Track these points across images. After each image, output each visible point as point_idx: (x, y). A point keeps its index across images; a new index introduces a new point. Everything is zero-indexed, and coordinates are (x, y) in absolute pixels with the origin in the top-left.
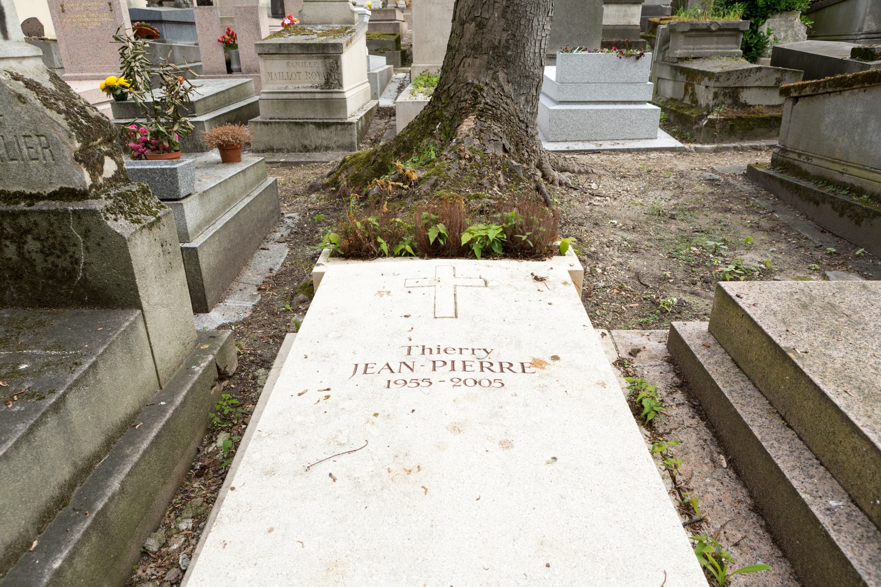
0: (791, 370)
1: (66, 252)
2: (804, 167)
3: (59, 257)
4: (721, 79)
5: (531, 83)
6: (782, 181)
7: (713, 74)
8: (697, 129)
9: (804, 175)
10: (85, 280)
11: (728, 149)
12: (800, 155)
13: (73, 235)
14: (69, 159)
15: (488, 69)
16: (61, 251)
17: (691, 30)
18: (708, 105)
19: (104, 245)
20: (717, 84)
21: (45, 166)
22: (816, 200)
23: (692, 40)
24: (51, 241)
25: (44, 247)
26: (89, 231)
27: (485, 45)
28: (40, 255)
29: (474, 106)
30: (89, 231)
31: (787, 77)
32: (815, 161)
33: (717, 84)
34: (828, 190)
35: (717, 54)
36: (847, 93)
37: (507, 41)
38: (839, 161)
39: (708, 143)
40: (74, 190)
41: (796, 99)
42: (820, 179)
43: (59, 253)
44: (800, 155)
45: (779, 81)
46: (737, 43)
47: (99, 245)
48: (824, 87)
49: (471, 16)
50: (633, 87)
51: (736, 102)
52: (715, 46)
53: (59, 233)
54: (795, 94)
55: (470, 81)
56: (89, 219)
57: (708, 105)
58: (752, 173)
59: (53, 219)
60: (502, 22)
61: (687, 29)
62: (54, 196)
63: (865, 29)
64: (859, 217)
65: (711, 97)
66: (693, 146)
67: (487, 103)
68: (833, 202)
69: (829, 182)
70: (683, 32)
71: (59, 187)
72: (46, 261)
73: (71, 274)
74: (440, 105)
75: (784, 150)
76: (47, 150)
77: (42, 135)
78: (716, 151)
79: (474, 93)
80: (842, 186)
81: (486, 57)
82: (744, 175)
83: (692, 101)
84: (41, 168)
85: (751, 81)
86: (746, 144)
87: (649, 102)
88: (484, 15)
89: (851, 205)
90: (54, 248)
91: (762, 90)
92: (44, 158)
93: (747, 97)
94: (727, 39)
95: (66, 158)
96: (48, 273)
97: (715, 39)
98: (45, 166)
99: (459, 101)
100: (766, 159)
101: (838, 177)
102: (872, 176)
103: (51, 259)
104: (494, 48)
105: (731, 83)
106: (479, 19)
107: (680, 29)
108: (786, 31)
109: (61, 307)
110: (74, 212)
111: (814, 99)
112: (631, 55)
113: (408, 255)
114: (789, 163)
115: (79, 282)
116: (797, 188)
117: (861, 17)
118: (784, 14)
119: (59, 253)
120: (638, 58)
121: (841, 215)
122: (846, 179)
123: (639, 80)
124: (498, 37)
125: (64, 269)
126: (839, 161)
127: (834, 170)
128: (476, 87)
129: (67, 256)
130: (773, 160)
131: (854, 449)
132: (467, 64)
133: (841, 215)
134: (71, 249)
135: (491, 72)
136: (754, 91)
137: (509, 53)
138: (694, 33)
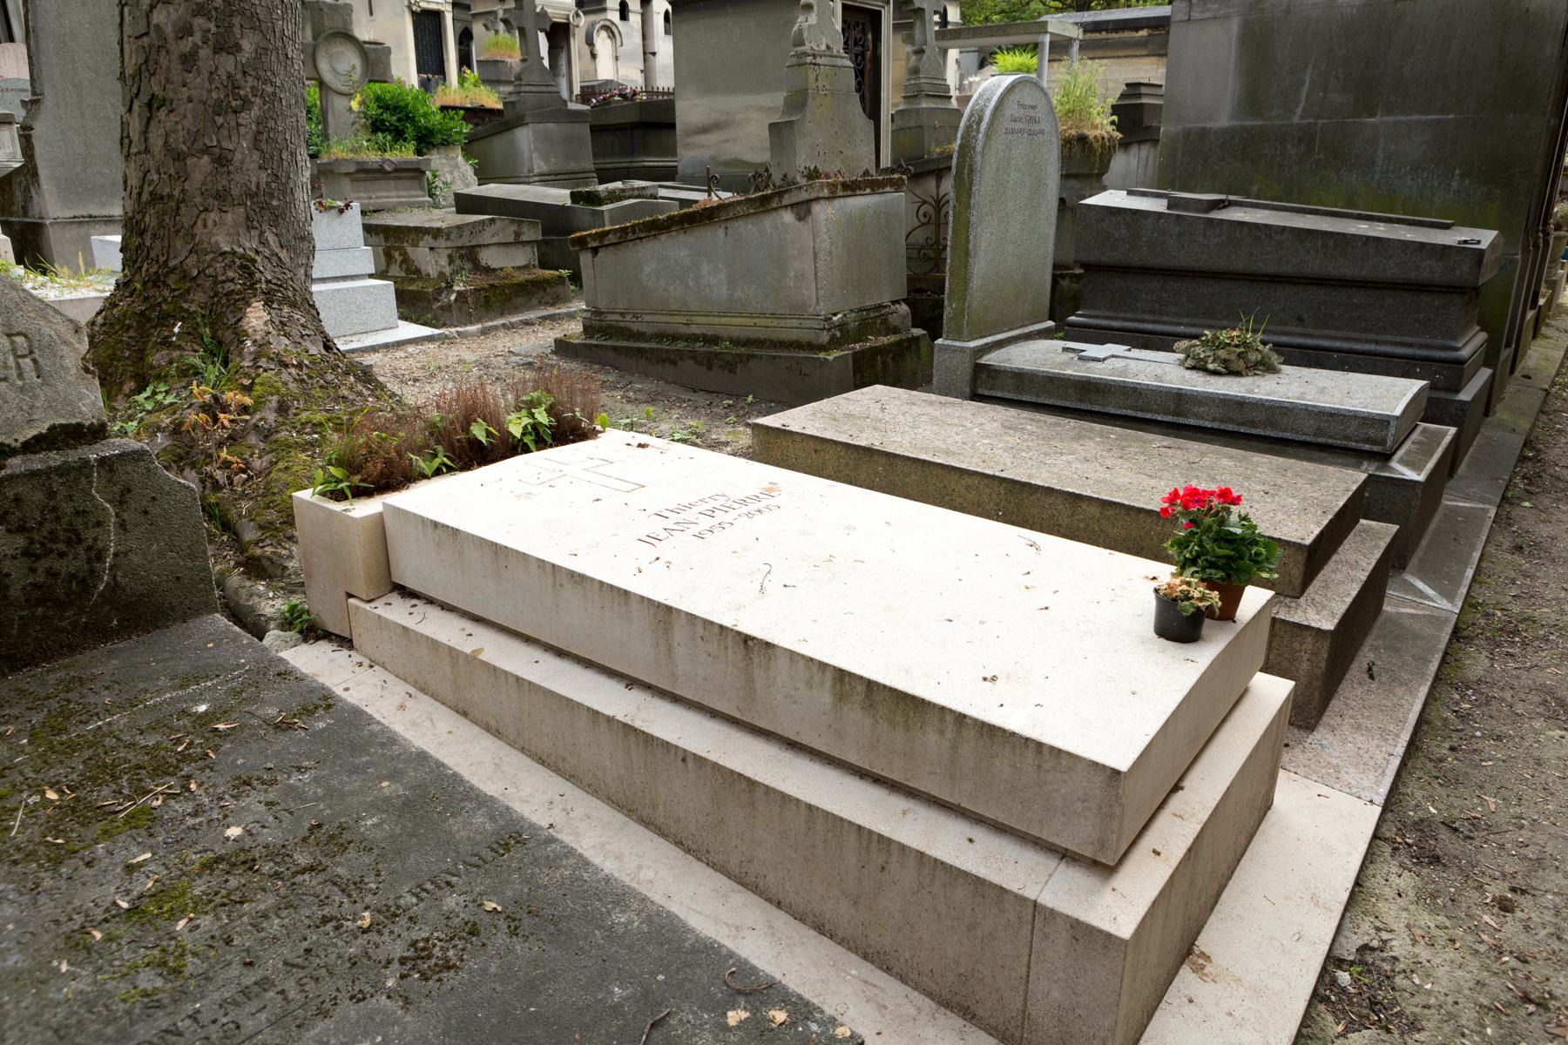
0: (883, 460)
1: (80, 541)
2: (635, 327)
3: (62, 555)
4: (453, 236)
5: (303, 245)
6: (615, 348)
7: (439, 230)
8: (442, 308)
9: (640, 336)
10: (114, 586)
11: (495, 328)
12: (622, 314)
13: (96, 507)
14: (74, 371)
15: (249, 228)
16: (69, 542)
17: (359, 171)
18: (441, 274)
19: (155, 511)
20: (449, 244)
21: (22, 389)
22: (672, 359)
23: (362, 185)
24: (48, 526)
25: (32, 542)
26: (129, 491)
27: (236, 191)
28: (24, 563)
29: (252, 287)
30: (129, 491)
31: (525, 228)
32: (647, 318)
33: (449, 244)
34: (681, 345)
35: (402, 204)
36: (663, 237)
37: (268, 184)
38: (679, 313)
39: (471, 323)
40: (79, 425)
41: (595, 251)
42: (660, 336)
43: (62, 547)
44: (622, 314)
45: (517, 234)
46: (422, 189)
47: (146, 512)
48: (634, 232)
49: (199, 145)
50: (345, 254)
51: (478, 268)
52: (394, 193)
53: (67, 508)
54: (595, 244)
55: (227, 249)
56: (129, 468)
57: (441, 274)
58: (563, 348)
59: (57, 483)
60: (256, 156)
61: (352, 169)
62: (31, 446)
63: (536, 171)
64: (730, 365)
65: (444, 261)
66: (453, 330)
67: (268, 282)
68: (694, 356)
69: (675, 338)
70: (346, 174)
71: (46, 426)
72: (33, 570)
73: (85, 582)
74: (166, 293)
75: (597, 313)
76: (27, 360)
77: (19, 334)
78: (484, 332)
79: (242, 267)
80: (694, 338)
81: (242, 210)
82: (553, 352)
83: (408, 271)
84: (11, 395)
85: (487, 237)
86: (515, 319)
87: (371, 276)
88: (225, 144)
89: (717, 354)
90: (55, 540)
91: (502, 248)
92: (20, 376)
93: (489, 258)
94: (408, 183)
95: (66, 369)
96: (37, 594)
97: (392, 183)
98: (22, 389)
99: (215, 282)
100: (575, 328)
101: (685, 330)
102: (723, 320)
103: (42, 565)
104: (252, 195)
105: (465, 241)
106: (217, 151)
107: (343, 170)
108: (451, 173)
109: (61, 656)
110: (102, 461)
111: (621, 247)
112: (331, 208)
113: (450, 470)
114: (609, 327)
115: (101, 595)
116: (640, 350)
117: (526, 155)
118: (442, 149)
119: (62, 547)
120: (341, 211)
121: (710, 368)
122: (694, 330)
123: (350, 244)
124: (254, 180)
125: (72, 577)
126: (679, 313)
127: (676, 323)
128: (243, 257)
129: (80, 550)
130: (586, 328)
131: (968, 488)
132: (210, 223)
133: (710, 368)
134: (89, 535)
135: (255, 233)
136: (493, 250)
137: (275, 203)
138: (362, 176)
